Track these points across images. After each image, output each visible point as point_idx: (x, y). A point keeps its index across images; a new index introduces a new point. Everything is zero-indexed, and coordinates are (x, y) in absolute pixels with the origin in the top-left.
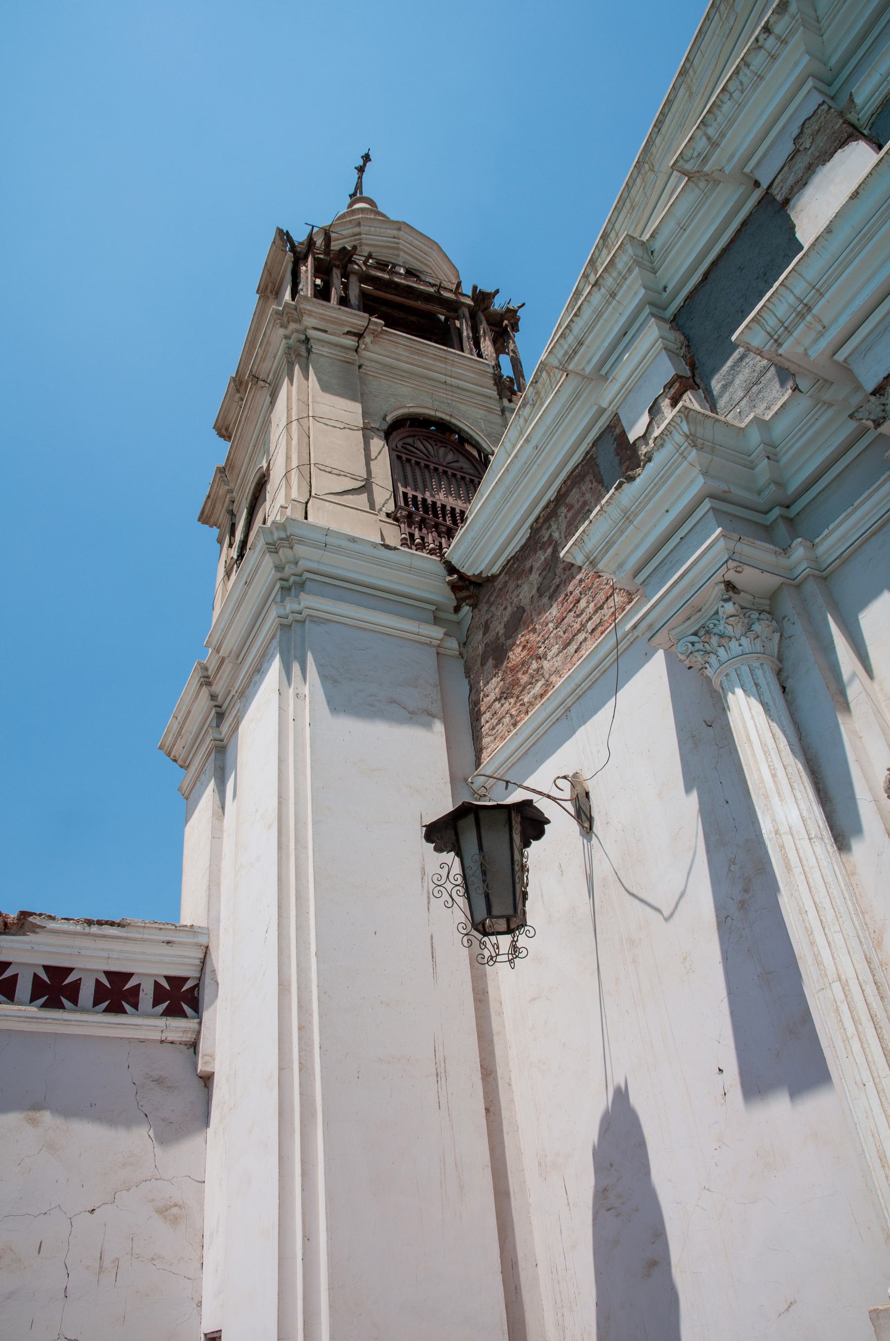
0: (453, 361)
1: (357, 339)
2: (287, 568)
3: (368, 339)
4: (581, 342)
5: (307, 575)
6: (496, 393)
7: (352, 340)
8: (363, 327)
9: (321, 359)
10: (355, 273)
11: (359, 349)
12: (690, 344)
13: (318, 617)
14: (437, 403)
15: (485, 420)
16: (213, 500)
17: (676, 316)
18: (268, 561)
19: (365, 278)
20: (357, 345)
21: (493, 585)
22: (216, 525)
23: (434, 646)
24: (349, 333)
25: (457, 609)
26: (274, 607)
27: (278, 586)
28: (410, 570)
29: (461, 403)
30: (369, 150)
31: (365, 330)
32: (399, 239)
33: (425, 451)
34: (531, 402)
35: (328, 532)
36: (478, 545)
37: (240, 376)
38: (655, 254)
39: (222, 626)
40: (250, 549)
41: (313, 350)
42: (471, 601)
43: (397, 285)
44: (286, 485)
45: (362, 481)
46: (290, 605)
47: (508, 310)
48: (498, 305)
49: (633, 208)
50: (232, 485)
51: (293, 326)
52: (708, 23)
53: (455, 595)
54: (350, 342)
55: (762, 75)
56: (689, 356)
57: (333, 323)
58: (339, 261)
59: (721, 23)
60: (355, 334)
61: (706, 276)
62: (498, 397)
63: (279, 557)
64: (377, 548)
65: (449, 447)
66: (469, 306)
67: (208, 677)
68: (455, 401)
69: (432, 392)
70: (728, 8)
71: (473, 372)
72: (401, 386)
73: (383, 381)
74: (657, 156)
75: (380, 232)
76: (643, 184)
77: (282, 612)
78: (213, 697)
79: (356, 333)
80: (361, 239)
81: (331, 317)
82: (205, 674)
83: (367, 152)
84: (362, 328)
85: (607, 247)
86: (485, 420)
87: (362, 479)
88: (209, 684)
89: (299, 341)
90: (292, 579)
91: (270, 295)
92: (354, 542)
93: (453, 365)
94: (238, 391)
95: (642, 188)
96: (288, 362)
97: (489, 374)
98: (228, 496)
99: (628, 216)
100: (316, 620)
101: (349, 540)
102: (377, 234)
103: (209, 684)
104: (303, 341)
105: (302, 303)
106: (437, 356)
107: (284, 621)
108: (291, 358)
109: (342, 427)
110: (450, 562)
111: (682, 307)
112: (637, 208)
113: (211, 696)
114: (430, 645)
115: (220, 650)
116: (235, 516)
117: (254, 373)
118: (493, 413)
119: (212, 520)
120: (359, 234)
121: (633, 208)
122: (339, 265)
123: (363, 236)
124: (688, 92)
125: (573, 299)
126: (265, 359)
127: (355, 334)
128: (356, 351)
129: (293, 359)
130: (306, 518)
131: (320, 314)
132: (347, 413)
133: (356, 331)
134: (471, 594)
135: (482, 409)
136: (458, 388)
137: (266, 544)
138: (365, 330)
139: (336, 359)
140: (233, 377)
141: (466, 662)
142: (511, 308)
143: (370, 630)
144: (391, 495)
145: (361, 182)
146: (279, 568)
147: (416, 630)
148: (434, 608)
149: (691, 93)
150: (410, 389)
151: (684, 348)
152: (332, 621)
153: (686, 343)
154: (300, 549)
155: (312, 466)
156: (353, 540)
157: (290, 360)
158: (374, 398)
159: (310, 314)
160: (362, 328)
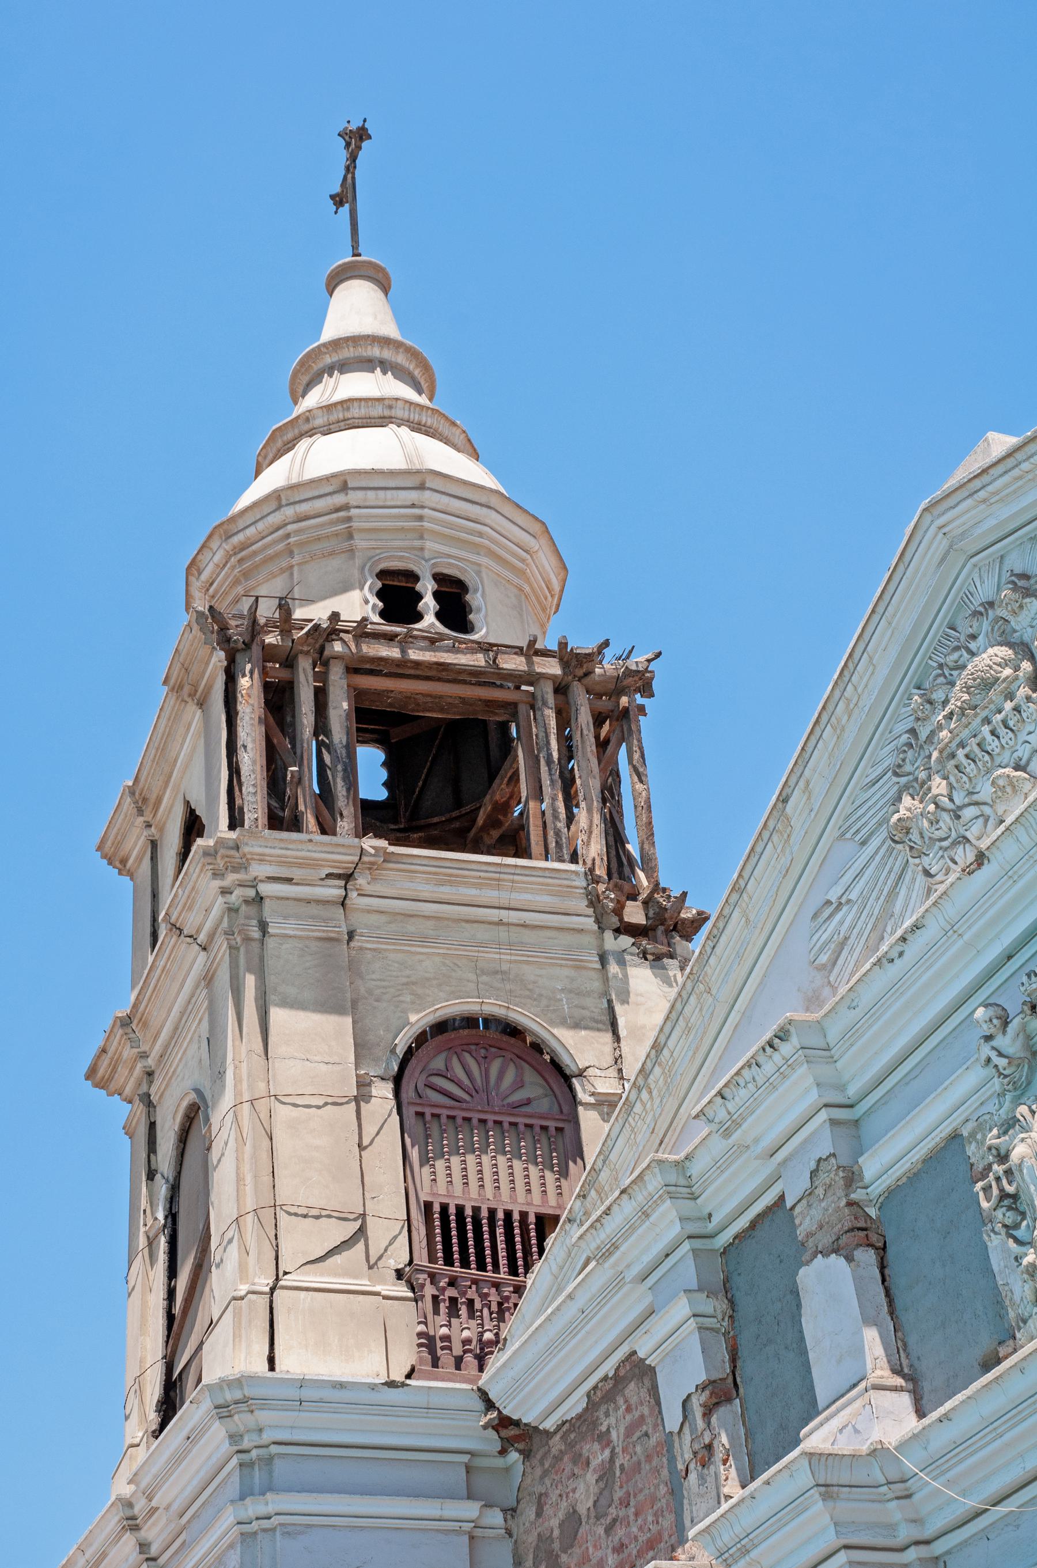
0: (513, 881)
1: (342, 883)
2: (246, 1439)
3: (361, 881)
4: (616, 1245)
5: (274, 1449)
6: (593, 919)
7: (335, 886)
8: (352, 863)
9: (284, 947)
10: (337, 657)
11: (347, 902)
12: (735, 1314)
13: (294, 1524)
14: (484, 978)
15: (570, 991)
16: (112, 1059)
17: (725, 1252)
18: (218, 1432)
19: (355, 668)
20: (344, 894)
21: (547, 1444)
22: (119, 1094)
23: (465, 1532)
24: (329, 876)
25: (503, 1452)
26: (230, 1509)
27: (234, 1461)
28: (427, 1413)
29: (527, 962)
30: (365, 121)
31: (355, 868)
32: (423, 507)
33: (466, 1082)
34: (578, 1221)
35: (302, 1383)
36: (522, 1390)
37: (143, 790)
38: (692, 1178)
39: (154, 1470)
40: (191, 1402)
41: (269, 930)
42: (521, 1446)
43: (417, 664)
44: (239, 1239)
45: (355, 1220)
46: (253, 1507)
47: (629, 673)
48: (607, 667)
49: (688, 1029)
50: (144, 1048)
51: (231, 878)
52: (753, 860)
53: (498, 1433)
54: (333, 891)
55: (775, 1084)
56: (732, 1333)
57: (300, 866)
58: (308, 645)
59: (776, 855)
60: (339, 876)
61: (753, 1225)
62: (595, 927)
63: (234, 1422)
64: (376, 1389)
65: (509, 1055)
66: (552, 678)
67: (133, 1518)
68: (516, 961)
69: (476, 954)
70: (783, 841)
71: (551, 894)
72: (422, 957)
73: (392, 956)
74: (713, 979)
75: (386, 500)
76: (699, 1006)
77: (243, 1516)
78: (143, 1546)
79: (340, 874)
80: (349, 519)
81: (296, 858)
82: (129, 1513)
83: (361, 125)
84: (350, 865)
85: (660, 1065)
86: (570, 991)
87: (355, 1216)
88: (135, 1528)
89: (246, 901)
90: (254, 1453)
91: (189, 700)
92: (342, 1388)
93: (512, 889)
94: (140, 812)
95: (698, 1009)
96: (230, 947)
97: (578, 891)
98: (139, 1066)
99: (684, 1037)
100: (290, 1532)
101: (334, 1387)
102: (381, 504)
103: (135, 1528)
104: (253, 899)
105: (247, 844)
106: (484, 878)
107: (246, 1528)
108: (235, 939)
109: (321, 1104)
110: (487, 1394)
111: (730, 1244)
112: (695, 1029)
113: (140, 1544)
114: (458, 1532)
115: (153, 1497)
116: (155, 1107)
117: (173, 920)
118: (585, 968)
119: (112, 1086)
120: (346, 507)
121: (688, 1029)
122: (309, 651)
123: (354, 512)
124: (744, 919)
125: (624, 1109)
126: (190, 908)
127: (339, 876)
128: (343, 904)
129: (239, 943)
130: (272, 1368)
131: (279, 856)
132: (330, 1066)
133: (341, 871)
134: (522, 1432)
135: (566, 966)
136: (524, 926)
137: (215, 1408)
138: (355, 868)
139: (308, 938)
140: (129, 787)
141: (516, 1541)
142: (634, 667)
143: (369, 1527)
144: (403, 1227)
145: (353, 178)
146: (234, 1437)
147: (436, 1513)
148: (465, 1458)
149: (748, 920)
150: (437, 959)
151: (726, 1319)
152: (313, 1525)
153: (729, 1312)
154: (263, 1417)
155: (278, 1208)
156: (341, 1385)
157: (233, 943)
158: (376, 1004)
159: (262, 859)
160: (350, 865)
